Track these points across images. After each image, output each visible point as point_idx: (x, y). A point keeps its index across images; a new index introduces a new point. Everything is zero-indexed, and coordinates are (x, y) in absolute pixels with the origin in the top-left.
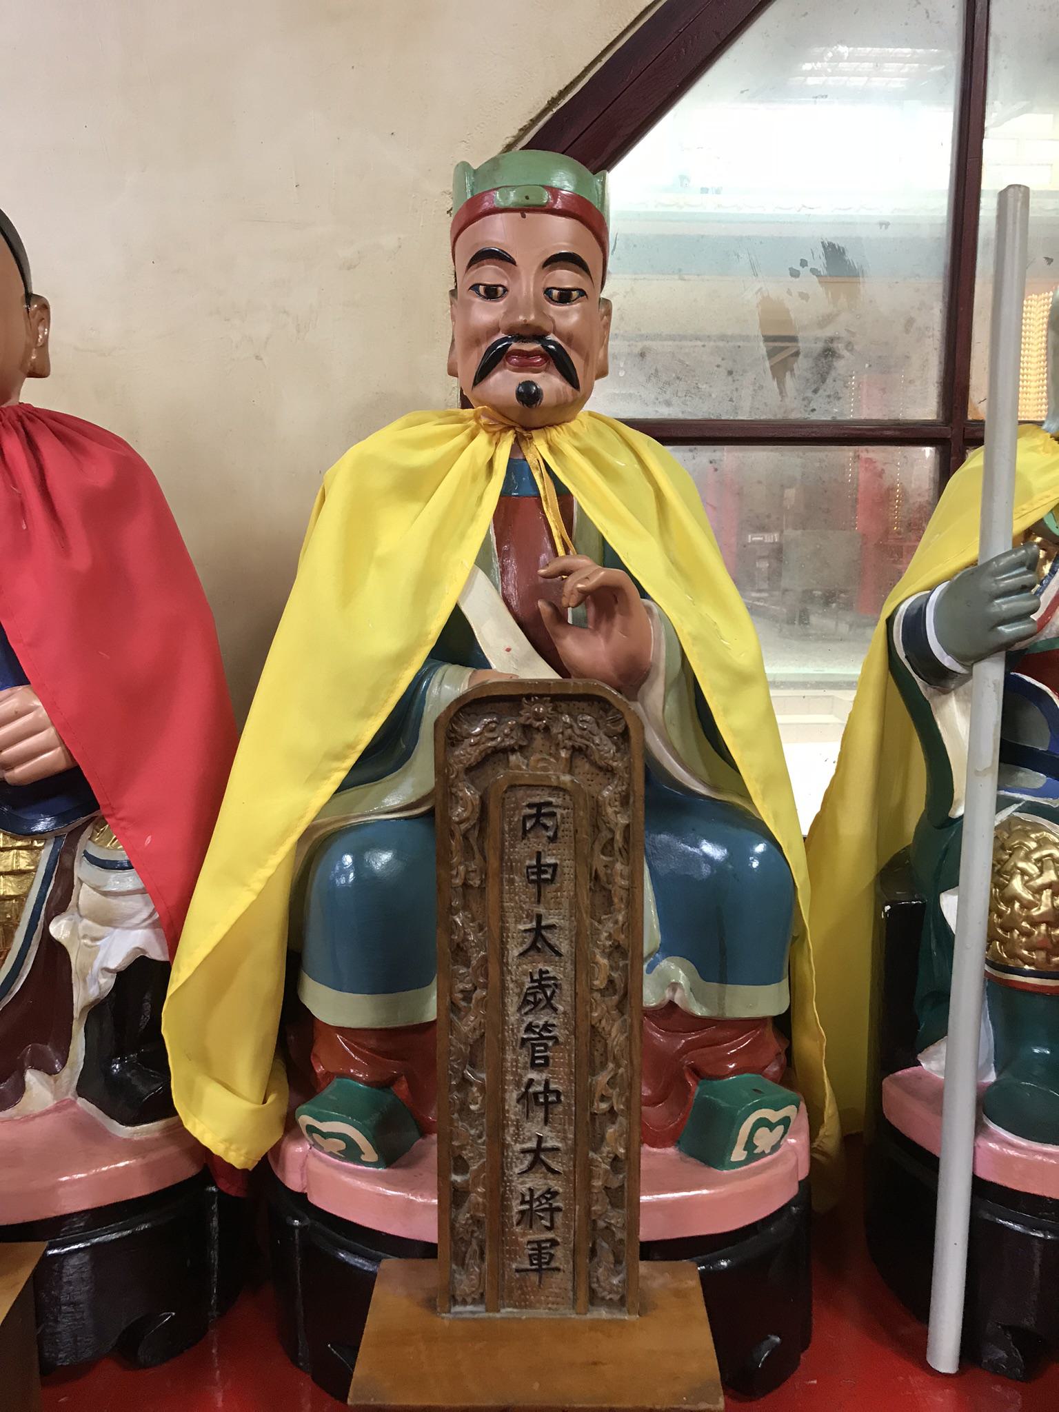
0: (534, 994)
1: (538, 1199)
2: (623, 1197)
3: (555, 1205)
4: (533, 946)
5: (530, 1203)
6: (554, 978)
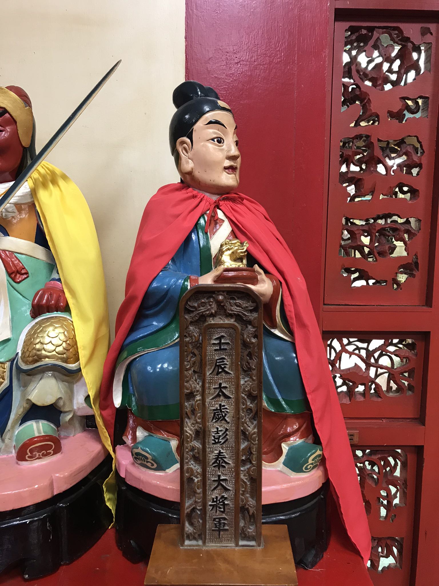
0: (218, 415)
1: (219, 501)
3: (226, 502)
4: (218, 396)
5: (216, 501)
6: (226, 408)
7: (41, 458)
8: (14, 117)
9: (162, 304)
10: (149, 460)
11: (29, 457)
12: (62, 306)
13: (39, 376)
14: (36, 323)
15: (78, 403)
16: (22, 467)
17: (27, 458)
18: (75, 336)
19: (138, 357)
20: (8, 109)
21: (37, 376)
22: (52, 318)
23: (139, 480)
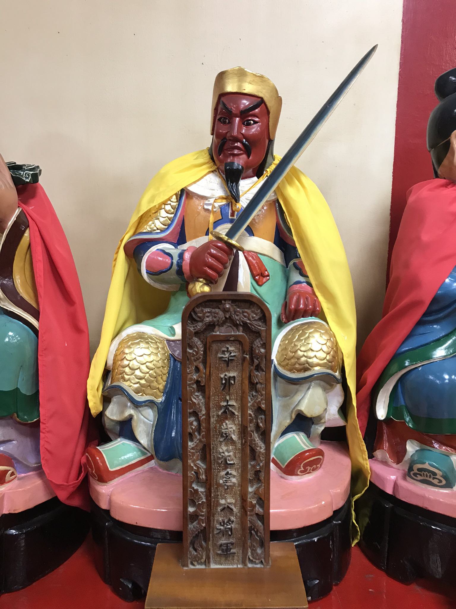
2: (264, 518)
7: (310, 473)
8: (269, 107)
9: (449, 310)
10: (437, 477)
11: (301, 472)
12: (301, 309)
13: (306, 386)
14: (292, 330)
15: (329, 414)
16: (290, 482)
17: (299, 473)
18: (337, 343)
19: (420, 366)
20: (265, 99)
21: (304, 385)
22: (311, 323)
23: (423, 497)
